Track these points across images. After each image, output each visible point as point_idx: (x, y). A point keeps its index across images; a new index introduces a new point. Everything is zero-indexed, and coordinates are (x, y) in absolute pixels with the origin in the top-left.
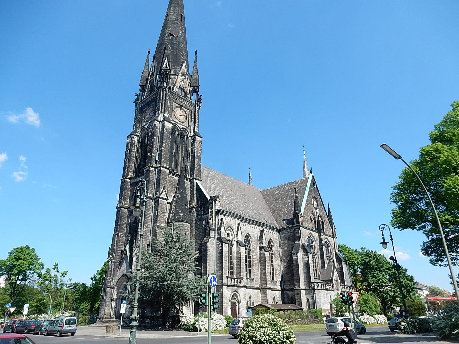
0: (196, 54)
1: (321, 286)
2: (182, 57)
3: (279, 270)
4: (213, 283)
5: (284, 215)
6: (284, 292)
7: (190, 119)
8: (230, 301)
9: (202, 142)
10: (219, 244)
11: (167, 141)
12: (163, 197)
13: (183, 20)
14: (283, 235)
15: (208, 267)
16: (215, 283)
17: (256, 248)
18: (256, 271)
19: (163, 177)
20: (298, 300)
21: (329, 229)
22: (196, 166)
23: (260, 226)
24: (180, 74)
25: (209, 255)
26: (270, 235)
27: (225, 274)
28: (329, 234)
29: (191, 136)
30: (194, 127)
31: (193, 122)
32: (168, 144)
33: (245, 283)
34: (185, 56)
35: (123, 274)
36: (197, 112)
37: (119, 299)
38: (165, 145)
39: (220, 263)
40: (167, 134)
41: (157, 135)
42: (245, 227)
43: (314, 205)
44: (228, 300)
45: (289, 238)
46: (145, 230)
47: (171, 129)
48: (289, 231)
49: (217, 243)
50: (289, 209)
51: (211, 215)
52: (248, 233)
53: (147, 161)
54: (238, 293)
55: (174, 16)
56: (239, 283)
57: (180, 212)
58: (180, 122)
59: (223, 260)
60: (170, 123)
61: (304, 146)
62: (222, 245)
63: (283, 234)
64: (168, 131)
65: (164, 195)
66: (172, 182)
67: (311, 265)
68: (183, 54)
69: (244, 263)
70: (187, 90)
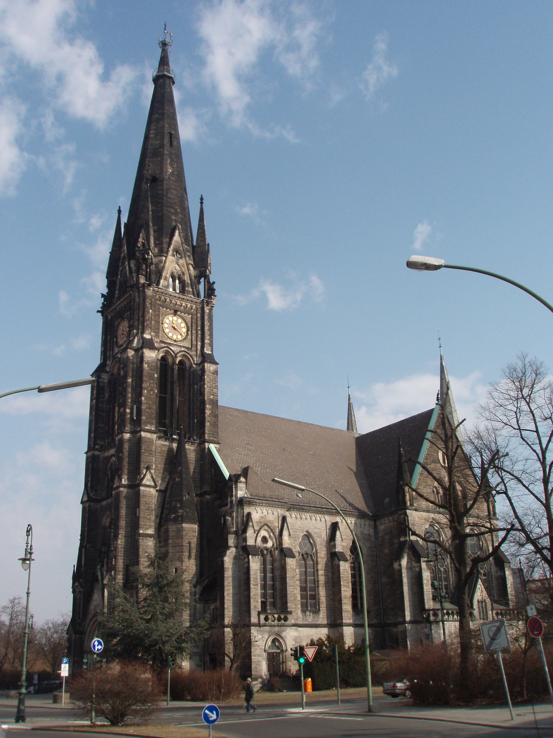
0: (202, 203)
9: (217, 372)
12: (148, 483)
13: (175, 143)
16: (100, 647)
19: (145, 449)
22: (207, 418)
27: (255, 607)
30: (203, 347)
31: (199, 336)
32: (151, 390)
34: (180, 213)
35: (257, 613)
36: (206, 317)
38: (146, 391)
40: (149, 371)
42: (299, 523)
48: (391, 518)
49: (242, 555)
51: (232, 507)
52: (307, 532)
54: (281, 637)
59: (251, 585)
64: (152, 366)
65: (148, 480)
68: (176, 210)
70: (187, 278)
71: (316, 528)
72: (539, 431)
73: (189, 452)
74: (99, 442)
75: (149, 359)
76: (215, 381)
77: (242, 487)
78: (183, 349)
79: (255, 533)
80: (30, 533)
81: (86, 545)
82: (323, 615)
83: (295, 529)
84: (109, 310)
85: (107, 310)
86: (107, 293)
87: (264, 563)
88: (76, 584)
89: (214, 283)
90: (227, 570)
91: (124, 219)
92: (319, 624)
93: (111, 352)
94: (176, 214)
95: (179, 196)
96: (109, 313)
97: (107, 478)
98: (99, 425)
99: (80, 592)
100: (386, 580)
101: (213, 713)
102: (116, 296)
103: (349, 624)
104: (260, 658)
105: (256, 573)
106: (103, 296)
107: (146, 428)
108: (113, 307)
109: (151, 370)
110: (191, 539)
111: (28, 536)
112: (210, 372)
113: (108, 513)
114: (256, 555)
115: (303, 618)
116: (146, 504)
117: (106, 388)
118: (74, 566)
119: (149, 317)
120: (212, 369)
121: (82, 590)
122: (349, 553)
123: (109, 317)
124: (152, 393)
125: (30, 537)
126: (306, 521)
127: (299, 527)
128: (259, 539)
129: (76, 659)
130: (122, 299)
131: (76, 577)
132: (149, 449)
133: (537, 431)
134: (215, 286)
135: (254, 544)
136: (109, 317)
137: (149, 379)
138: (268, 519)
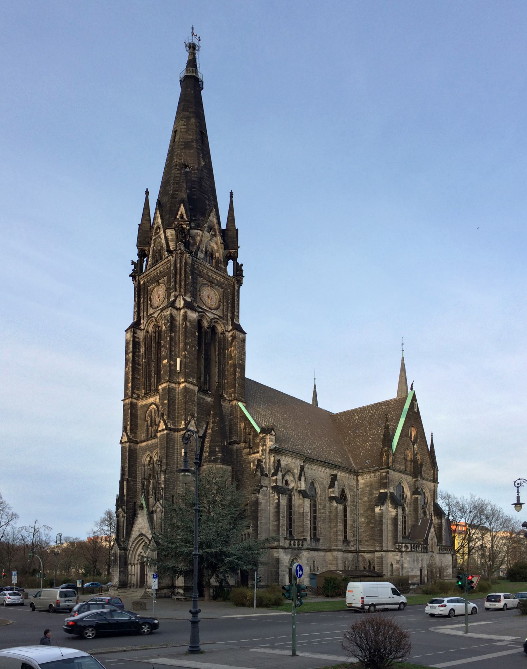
1: (411, 548)
2: (207, 202)
3: (355, 527)
5: (365, 452)
6: (359, 554)
7: (225, 304)
10: (275, 496)
11: (192, 341)
14: (363, 481)
15: (259, 525)
17: (324, 499)
18: (323, 529)
21: (429, 472)
23: (331, 468)
24: (206, 229)
25: (261, 510)
26: (344, 481)
27: (283, 534)
28: (428, 478)
29: (229, 330)
32: (193, 346)
33: (309, 545)
37: (137, 564)
38: (189, 347)
39: (276, 521)
43: (411, 438)
44: (286, 566)
45: (371, 485)
46: (168, 477)
47: (196, 321)
48: (372, 475)
49: (272, 493)
50: (373, 443)
53: (162, 372)
55: (189, 135)
56: (301, 546)
57: (217, 451)
58: (210, 308)
60: (196, 311)
61: (403, 344)
62: (279, 497)
63: (362, 479)
64: (193, 325)
66: (202, 405)
67: (400, 521)
68: (209, 197)
69: (308, 520)
71: (320, 477)
72: (308, 451)
74: (136, 391)
75: (191, 319)
78: (216, 317)
85: (140, 276)
86: (138, 261)
88: (119, 510)
89: (242, 265)
92: (319, 549)
93: (145, 313)
96: (141, 278)
97: (146, 423)
98: (136, 376)
100: (363, 520)
104: (285, 573)
105: (283, 509)
106: (133, 263)
107: (189, 380)
117: (141, 344)
123: (142, 283)
126: (314, 472)
127: (310, 475)
129: (122, 569)
132: (192, 399)
134: (243, 268)
136: (142, 283)
137: (191, 336)
138: (290, 467)
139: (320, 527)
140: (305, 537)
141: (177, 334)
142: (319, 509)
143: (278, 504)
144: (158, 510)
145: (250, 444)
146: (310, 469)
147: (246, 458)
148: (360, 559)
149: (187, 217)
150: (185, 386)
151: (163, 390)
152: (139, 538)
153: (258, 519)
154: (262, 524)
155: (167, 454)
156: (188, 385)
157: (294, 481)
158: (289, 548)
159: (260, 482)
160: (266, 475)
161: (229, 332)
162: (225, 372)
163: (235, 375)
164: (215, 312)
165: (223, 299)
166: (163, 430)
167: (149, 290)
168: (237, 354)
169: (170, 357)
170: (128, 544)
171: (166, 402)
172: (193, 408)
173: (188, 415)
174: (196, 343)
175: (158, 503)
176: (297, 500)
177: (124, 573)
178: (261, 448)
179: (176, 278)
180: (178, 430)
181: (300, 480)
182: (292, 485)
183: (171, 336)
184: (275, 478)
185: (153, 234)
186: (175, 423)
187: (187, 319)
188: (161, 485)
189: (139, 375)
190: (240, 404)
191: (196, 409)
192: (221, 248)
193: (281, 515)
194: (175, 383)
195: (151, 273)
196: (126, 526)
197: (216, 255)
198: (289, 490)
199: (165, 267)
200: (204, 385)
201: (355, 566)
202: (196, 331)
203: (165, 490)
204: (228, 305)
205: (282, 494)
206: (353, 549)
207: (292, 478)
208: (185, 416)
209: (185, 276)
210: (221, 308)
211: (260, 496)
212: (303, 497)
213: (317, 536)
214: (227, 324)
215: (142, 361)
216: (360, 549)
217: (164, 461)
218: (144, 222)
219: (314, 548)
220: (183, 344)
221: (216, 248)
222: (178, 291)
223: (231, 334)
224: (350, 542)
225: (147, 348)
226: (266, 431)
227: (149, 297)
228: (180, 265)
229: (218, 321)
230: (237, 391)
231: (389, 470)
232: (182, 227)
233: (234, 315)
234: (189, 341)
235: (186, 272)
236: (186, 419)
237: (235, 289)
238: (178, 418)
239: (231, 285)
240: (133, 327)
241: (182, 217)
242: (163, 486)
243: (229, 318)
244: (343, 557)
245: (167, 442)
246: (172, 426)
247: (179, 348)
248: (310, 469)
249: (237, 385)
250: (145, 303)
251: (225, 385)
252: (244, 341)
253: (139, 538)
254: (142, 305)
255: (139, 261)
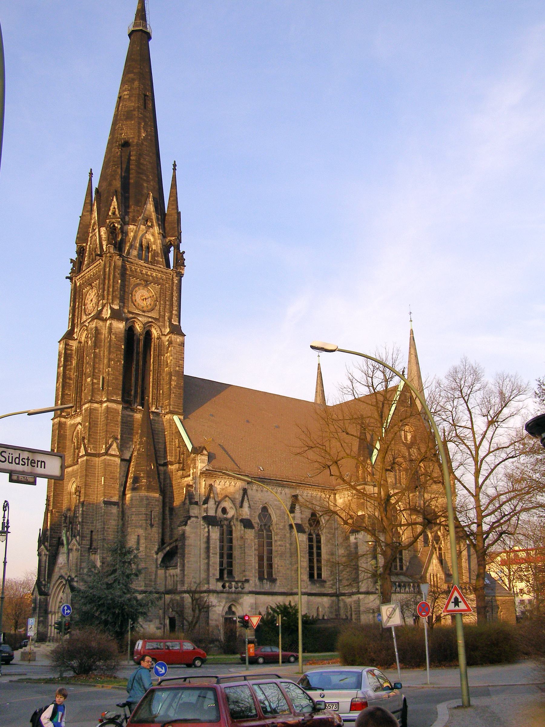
0: (174, 169)
4: (66, 612)
7: (162, 302)
8: (223, 616)
12: (113, 453)
16: (69, 611)
18: (281, 566)
20: (355, 611)
25: (188, 545)
27: (214, 575)
32: (118, 361)
34: (152, 180)
37: (58, 612)
41: (101, 345)
44: (219, 614)
49: (203, 525)
58: (144, 312)
63: (340, 498)
68: (148, 177)
73: (154, 423)
76: (181, 353)
77: (204, 459)
78: (150, 320)
79: (215, 504)
80: (7, 508)
81: (52, 510)
82: (280, 584)
83: (256, 501)
84: (78, 277)
85: (76, 277)
87: (222, 534)
89: (184, 252)
90: (187, 539)
91: (95, 184)
94: (148, 181)
95: (151, 161)
96: (78, 280)
97: (73, 445)
98: (66, 392)
99: (45, 555)
101: (162, 669)
102: (86, 262)
103: (305, 593)
106: (72, 261)
107: (112, 398)
108: (83, 274)
109: (119, 341)
110: (154, 508)
111: (5, 511)
112: (177, 344)
113: (74, 479)
114: (216, 526)
115: (260, 586)
116: (111, 473)
118: (40, 529)
119: (117, 287)
120: (178, 340)
121: (48, 553)
122: (307, 525)
123: (78, 284)
124: (118, 364)
125: (6, 512)
127: (260, 499)
128: (220, 510)
129: (41, 619)
130: (91, 267)
131: (42, 541)
133: (472, 429)
134: (185, 256)
135: (214, 515)
136: (78, 284)
139: (277, 564)
140: (247, 578)
141: (102, 349)
142: (276, 541)
143: (208, 538)
144: (75, 547)
145: (183, 465)
146: (259, 492)
147: (180, 482)
148: (341, 604)
149: (119, 213)
150: (107, 406)
151: (85, 411)
152: (60, 581)
153: (184, 556)
154: (190, 563)
155: (85, 483)
156: (110, 405)
157: (234, 507)
158: (222, 592)
159: (188, 511)
160: (196, 503)
161: (166, 335)
162: (160, 382)
163: (170, 385)
164: (149, 315)
165: (160, 297)
166: (82, 456)
167: (84, 293)
168: (173, 360)
169: (93, 375)
170: (49, 588)
171: (87, 424)
172: (116, 430)
173: (110, 438)
174: (122, 357)
175: (74, 540)
176: (238, 530)
177: (43, 624)
178: (192, 471)
179: (104, 285)
180: (99, 455)
181: (241, 506)
182: (231, 513)
183: (95, 352)
184: (206, 506)
185: (90, 231)
186: (96, 447)
187: (111, 332)
188: (78, 519)
189: (70, 390)
190: (176, 418)
191: (119, 430)
192: (159, 239)
193: (211, 551)
194: (97, 403)
195: (86, 275)
196: (49, 566)
197: (152, 249)
198: (226, 519)
199: (97, 269)
200: (135, 399)
201: (334, 614)
202: (123, 343)
203: (82, 525)
204: (165, 302)
205: (212, 525)
206: (330, 591)
207: (231, 505)
208: (106, 440)
209: (114, 282)
210: (157, 308)
211: (187, 528)
212: (245, 527)
213: (274, 576)
214: (164, 326)
215: (73, 374)
216: (340, 591)
217: (83, 491)
218: (84, 214)
219: (268, 591)
220: (107, 359)
221: (152, 240)
222: (106, 298)
223: (167, 338)
224: (325, 582)
225: (79, 360)
226: (197, 450)
227: (83, 301)
228: (109, 269)
229: (153, 324)
230: (172, 403)
231: (366, 486)
232: (114, 226)
233: (172, 314)
234: (112, 356)
235: (114, 276)
236: (106, 443)
237: (174, 283)
238: (100, 442)
239: (169, 279)
240: (66, 338)
241: (114, 213)
242: (80, 520)
243: (166, 318)
244: (308, 602)
245: (86, 470)
246: (93, 452)
247: (104, 364)
248: (259, 492)
249: (173, 395)
250: (80, 308)
251: (160, 396)
252: (182, 344)
253: (60, 581)
254: (77, 310)
255: (77, 259)
